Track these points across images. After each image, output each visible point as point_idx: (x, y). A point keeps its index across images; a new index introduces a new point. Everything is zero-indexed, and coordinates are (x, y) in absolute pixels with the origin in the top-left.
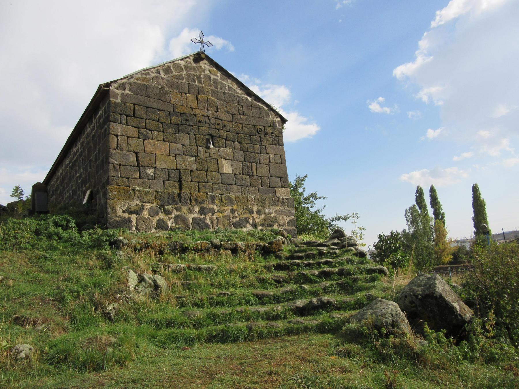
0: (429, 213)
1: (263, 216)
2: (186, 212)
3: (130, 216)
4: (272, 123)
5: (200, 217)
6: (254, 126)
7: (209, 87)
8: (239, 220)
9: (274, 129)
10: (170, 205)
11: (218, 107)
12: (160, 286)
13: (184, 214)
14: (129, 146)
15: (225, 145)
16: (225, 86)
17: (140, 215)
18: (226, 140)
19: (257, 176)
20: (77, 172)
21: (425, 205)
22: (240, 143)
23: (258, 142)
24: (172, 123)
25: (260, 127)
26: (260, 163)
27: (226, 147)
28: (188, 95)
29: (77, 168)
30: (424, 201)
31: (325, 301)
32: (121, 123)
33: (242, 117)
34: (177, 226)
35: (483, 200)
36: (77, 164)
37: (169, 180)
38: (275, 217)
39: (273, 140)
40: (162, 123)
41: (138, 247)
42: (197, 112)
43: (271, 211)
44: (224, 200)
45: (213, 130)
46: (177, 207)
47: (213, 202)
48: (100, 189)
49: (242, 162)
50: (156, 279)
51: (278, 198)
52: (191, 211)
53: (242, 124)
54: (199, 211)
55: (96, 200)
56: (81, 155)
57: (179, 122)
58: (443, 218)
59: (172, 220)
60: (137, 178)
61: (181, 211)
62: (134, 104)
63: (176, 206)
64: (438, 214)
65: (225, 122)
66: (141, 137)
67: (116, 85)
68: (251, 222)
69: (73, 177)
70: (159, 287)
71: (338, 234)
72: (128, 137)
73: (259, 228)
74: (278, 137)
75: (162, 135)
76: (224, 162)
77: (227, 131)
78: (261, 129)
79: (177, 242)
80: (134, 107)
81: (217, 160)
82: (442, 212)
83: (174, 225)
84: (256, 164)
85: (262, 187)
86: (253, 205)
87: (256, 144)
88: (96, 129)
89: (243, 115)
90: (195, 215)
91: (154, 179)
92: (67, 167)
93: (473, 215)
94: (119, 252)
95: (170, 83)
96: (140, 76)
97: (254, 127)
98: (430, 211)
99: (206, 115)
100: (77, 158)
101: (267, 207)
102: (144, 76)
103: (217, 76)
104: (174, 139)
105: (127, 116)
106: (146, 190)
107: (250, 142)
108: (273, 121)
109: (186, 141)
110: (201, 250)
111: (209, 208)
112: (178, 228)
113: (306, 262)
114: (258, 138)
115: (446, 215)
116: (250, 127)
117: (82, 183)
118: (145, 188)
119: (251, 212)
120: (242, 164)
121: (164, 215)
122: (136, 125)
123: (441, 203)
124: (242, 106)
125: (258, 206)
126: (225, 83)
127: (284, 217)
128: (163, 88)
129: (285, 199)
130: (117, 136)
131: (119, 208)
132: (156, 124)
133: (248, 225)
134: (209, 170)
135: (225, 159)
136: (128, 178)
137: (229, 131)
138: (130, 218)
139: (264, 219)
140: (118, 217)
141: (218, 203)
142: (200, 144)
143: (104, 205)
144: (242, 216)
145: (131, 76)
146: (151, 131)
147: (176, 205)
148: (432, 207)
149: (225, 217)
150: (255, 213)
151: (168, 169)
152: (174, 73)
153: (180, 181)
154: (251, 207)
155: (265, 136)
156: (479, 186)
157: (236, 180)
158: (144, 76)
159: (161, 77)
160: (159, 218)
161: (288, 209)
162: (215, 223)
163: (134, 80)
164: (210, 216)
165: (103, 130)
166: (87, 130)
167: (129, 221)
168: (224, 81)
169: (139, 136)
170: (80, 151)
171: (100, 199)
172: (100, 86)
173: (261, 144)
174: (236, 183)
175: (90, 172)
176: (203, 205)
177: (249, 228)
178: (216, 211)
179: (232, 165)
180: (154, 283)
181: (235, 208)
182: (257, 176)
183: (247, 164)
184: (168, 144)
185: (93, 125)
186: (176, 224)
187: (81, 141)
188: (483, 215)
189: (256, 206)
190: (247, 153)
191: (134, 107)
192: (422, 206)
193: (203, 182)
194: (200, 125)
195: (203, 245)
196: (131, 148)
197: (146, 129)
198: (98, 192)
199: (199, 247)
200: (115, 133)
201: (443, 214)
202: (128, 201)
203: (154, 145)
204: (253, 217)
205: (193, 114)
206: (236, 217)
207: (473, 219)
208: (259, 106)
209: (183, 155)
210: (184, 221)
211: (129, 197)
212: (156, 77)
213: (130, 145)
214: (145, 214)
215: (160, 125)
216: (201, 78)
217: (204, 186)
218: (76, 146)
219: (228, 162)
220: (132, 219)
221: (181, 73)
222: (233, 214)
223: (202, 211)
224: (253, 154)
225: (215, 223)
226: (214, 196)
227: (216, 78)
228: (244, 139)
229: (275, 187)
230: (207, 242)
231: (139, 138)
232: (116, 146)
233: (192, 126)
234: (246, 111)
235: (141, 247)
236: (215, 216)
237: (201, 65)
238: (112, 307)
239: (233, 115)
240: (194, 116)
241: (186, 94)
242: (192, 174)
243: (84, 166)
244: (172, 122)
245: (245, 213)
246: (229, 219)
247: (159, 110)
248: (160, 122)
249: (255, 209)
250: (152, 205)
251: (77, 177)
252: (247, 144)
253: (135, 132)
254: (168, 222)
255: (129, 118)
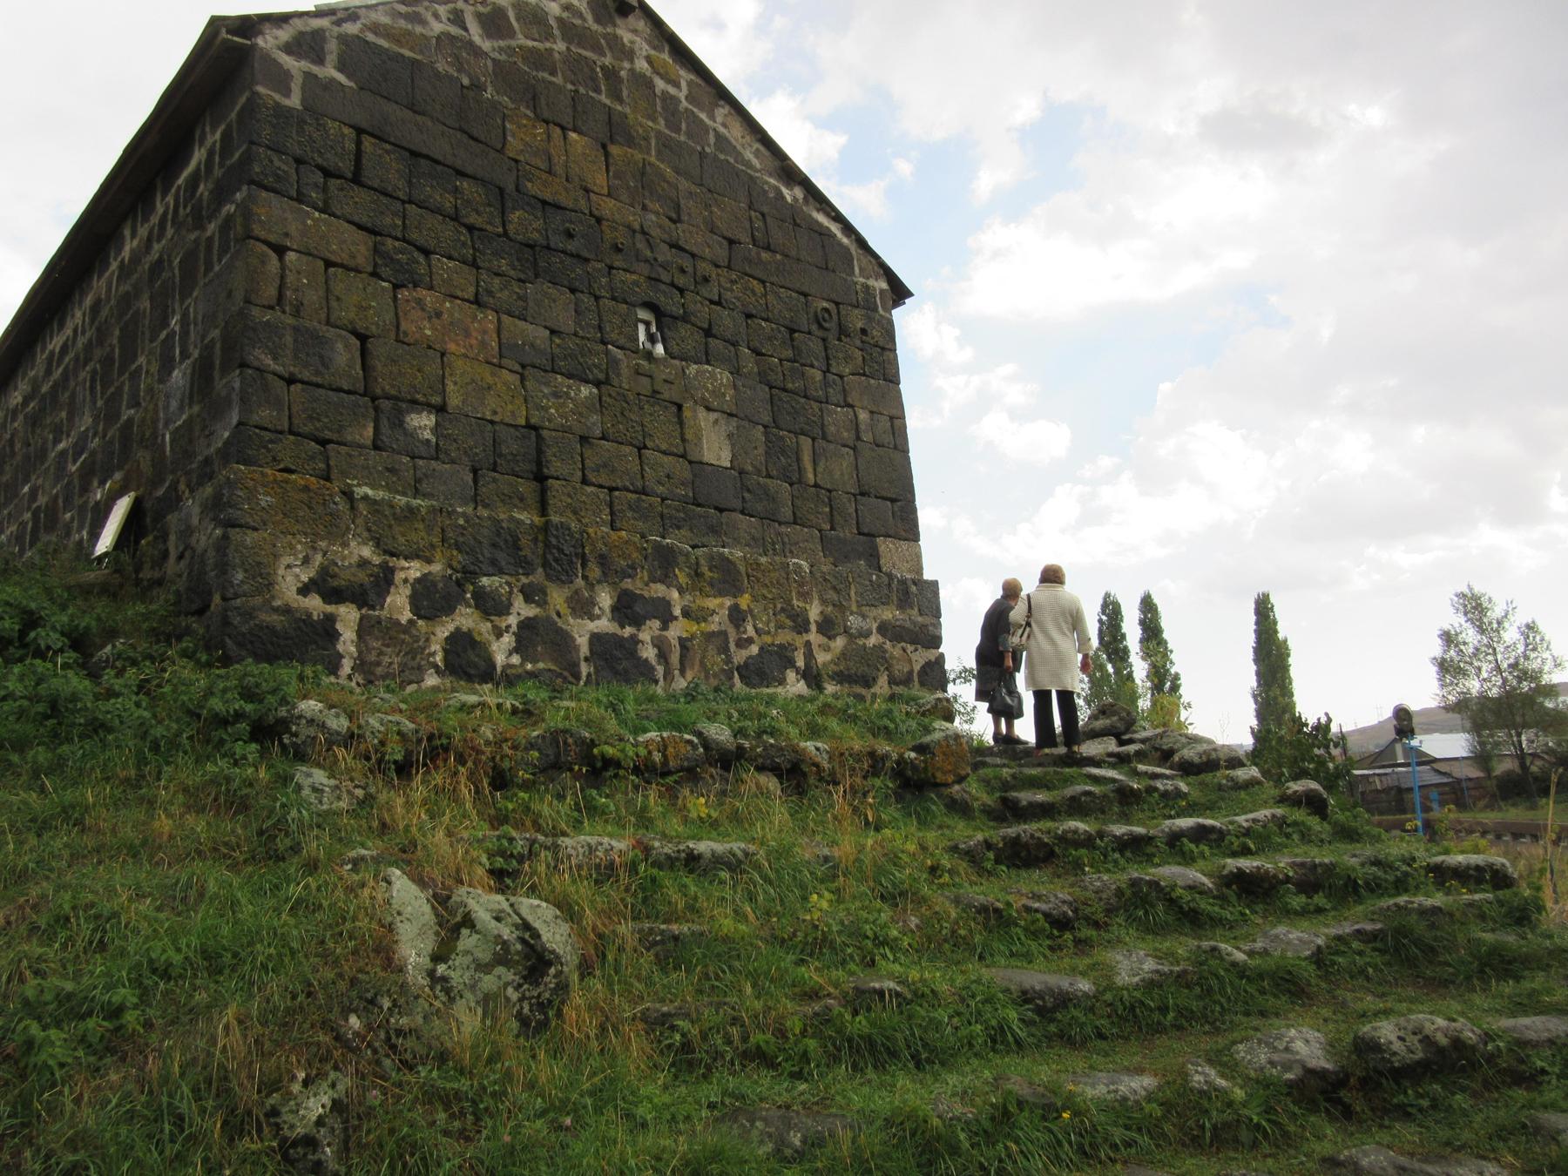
0: (1135, 675)
1: (840, 642)
2: (564, 609)
3: (330, 609)
4: (861, 296)
5: (619, 632)
6: (805, 295)
7: (650, 124)
8: (759, 655)
9: (870, 319)
10: (501, 572)
11: (682, 202)
12: (558, 957)
13: (558, 614)
14: (334, 304)
15: (707, 354)
16: (706, 129)
17: (373, 608)
18: (708, 333)
19: (816, 485)
20: (58, 436)
21: (1126, 651)
22: (758, 353)
23: (817, 359)
24: (511, 234)
25: (825, 304)
26: (824, 437)
27: (708, 363)
28: (573, 135)
29: (64, 414)
30: (1123, 636)
31: (1443, 1041)
32: (300, 198)
33: (765, 255)
34: (529, 666)
35: (1285, 641)
36: (65, 397)
37: (494, 470)
38: (879, 648)
39: (867, 357)
40: (471, 228)
41: (396, 753)
42: (608, 207)
43: (865, 625)
44: (705, 569)
45: (663, 287)
46: (530, 585)
47: (666, 579)
48: (182, 487)
49: (765, 427)
50: (530, 919)
51: (890, 576)
52: (584, 608)
53: (763, 282)
54: (614, 609)
55: (164, 537)
56: (80, 362)
57: (536, 236)
58: (1175, 688)
59: (508, 640)
60: (365, 447)
61: (543, 604)
62: (360, 131)
63: (524, 580)
64: (1163, 680)
65: (704, 265)
66: (385, 271)
67: (284, 34)
68: (800, 663)
69: (42, 454)
70: (549, 964)
71: (1115, 718)
72: (329, 264)
73: (830, 688)
74: (883, 349)
75: (472, 279)
76: (704, 419)
77: (712, 302)
78: (826, 310)
79: (565, 731)
80: (359, 143)
81: (680, 407)
82: (1173, 671)
83: (516, 659)
84: (814, 439)
85: (832, 528)
86: (805, 596)
87: (812, 366)
88: (170, 232)
89: (768, 248)
90: (597, 622)
91: (437, 459)
92: (14, 420)
93: (1255, 684)
94: (309, 775)
95: (502, 72)
96: (385, 20)
97: (802, 299)
98: (1140, 669)
99: (637, 227)
100: (66, 370)
101: (854, 608)
102: (402, 23)
103: (677, 85)
104: (520, 303)
105: (327, 173)
106: (401, 500)
107: (789, 353)
108: (867, 288)
109: (563, 316)
110: (664, 774)
111: (652, 599)
112: (532, 675)
113: (1119, 830)
114: (815, 346)
115: (1183, 681)
116: (791, 296)
117: (87, 474)
118: (397, 492)
119: (801, 626)
120: (766, 434)
121: (477, 615)
122: (364, 220)
123: (1170, 646)
124: (763, 215)
125: (824, 602)
126: (703, 116)
127: (910, 648)
128: (477, 87)
129: (909, 583)
130: (280, 251)
131: (281, 572)
132: (447, 231)
133: (791, 675)
134: (649, 444)
135: (708, 409)
136: (323, 443)
137: (719, 303)
138: (330, 619)
139: (844, 655)
140: (276, 610)
141: (683, 579)
142: (614, 336)
143: (211, 553)
144: (768, 639)
145: (351, 15)
146: (427, 253)
147: (526, 575)
148: (1147, 654)
149: (709, 636)
150: (813, 627)
151: (492, 422)
152: (521, 40)
153: (540, 478)
154: (801, 604)
155: (839, 339)
156: (1272, 599)
157: (747, 495)
158: (402, 23)
159: (471, 43)
160: (458, 629)
161: (920, 619)
162: (675, 658)
163: (361, 31)
164: (657, 633)
165: (212, 228)
166: (120, 250)
167: (327, 631)
168: (702, 110)
169: (376, 265)
170: (81, 341)
171: (187, 532)
172: (215, 23)
173: (828, 365)
174: (748, 505)
175: (130, 421)
176: (627, 584)
177: (795, 686)
178: (677, 612)
179: (730, 436)
180: (522, 941)
181: (744, 607)
182: (816, 485)
183: (782, 438)
184: (491, 316)
185: (155, 219)
186: (524, 660)
187: (89, 301)
188: (1283, 681)
189: (816, 602)
190: (783, 395)
191: (359, 143)
192: (1116, 651)
193: (628, 490)
194: (617, 264)
195: (670, 750)
196: (346, 314)
197: (404, 240)
198: (173, 501)
199: (657, 757)
200: (272, 238)
201: (1177, 677)
202: (323, 544)
203: (438, 315)
204: (808, 644)
205: (591, 215)
206: (750, 641)
207: (1255, 697)
208: (820, 225)
209: (553, 371)
210: (561, 643)
211: (335, 530)
212: (452, 38)
213: (338, 299)
214: (398, 604)
215: (465, 236)
216: (620, 80)
217: (630, 507)
218: (61, 326)
219: (716, 422)
220: (339, 626)
221: (548, 45)
222: (737, 627)
223: (626, 609)
224: (803, 400)
225: (675, 658)
226: (670, 550)
227: (672, 90)
228: (770, 339)
229: (874, 536)
230: (687, 737)
231: (375, 274)
232: (272, 291)
233: (587, 260)
234: (778, 237)
235: (408, 754)
236: (675, 632)
237: (619, 32)
238: (326, 1099)
239: (731, 242)
240: (593, 221)
241: (563, 128)
242: (588, 453)
243: (100, 403)
244: (511, 228)
245: (780, 626)
246: (724, 649)
247: (460, 173)
248: (465, 225)
249: (814, 612)
250: (427, 569)
251: (63, 453)
252: (781, 360)
253: (362, 248)
254: (495, 647)
255: (334, 183)
